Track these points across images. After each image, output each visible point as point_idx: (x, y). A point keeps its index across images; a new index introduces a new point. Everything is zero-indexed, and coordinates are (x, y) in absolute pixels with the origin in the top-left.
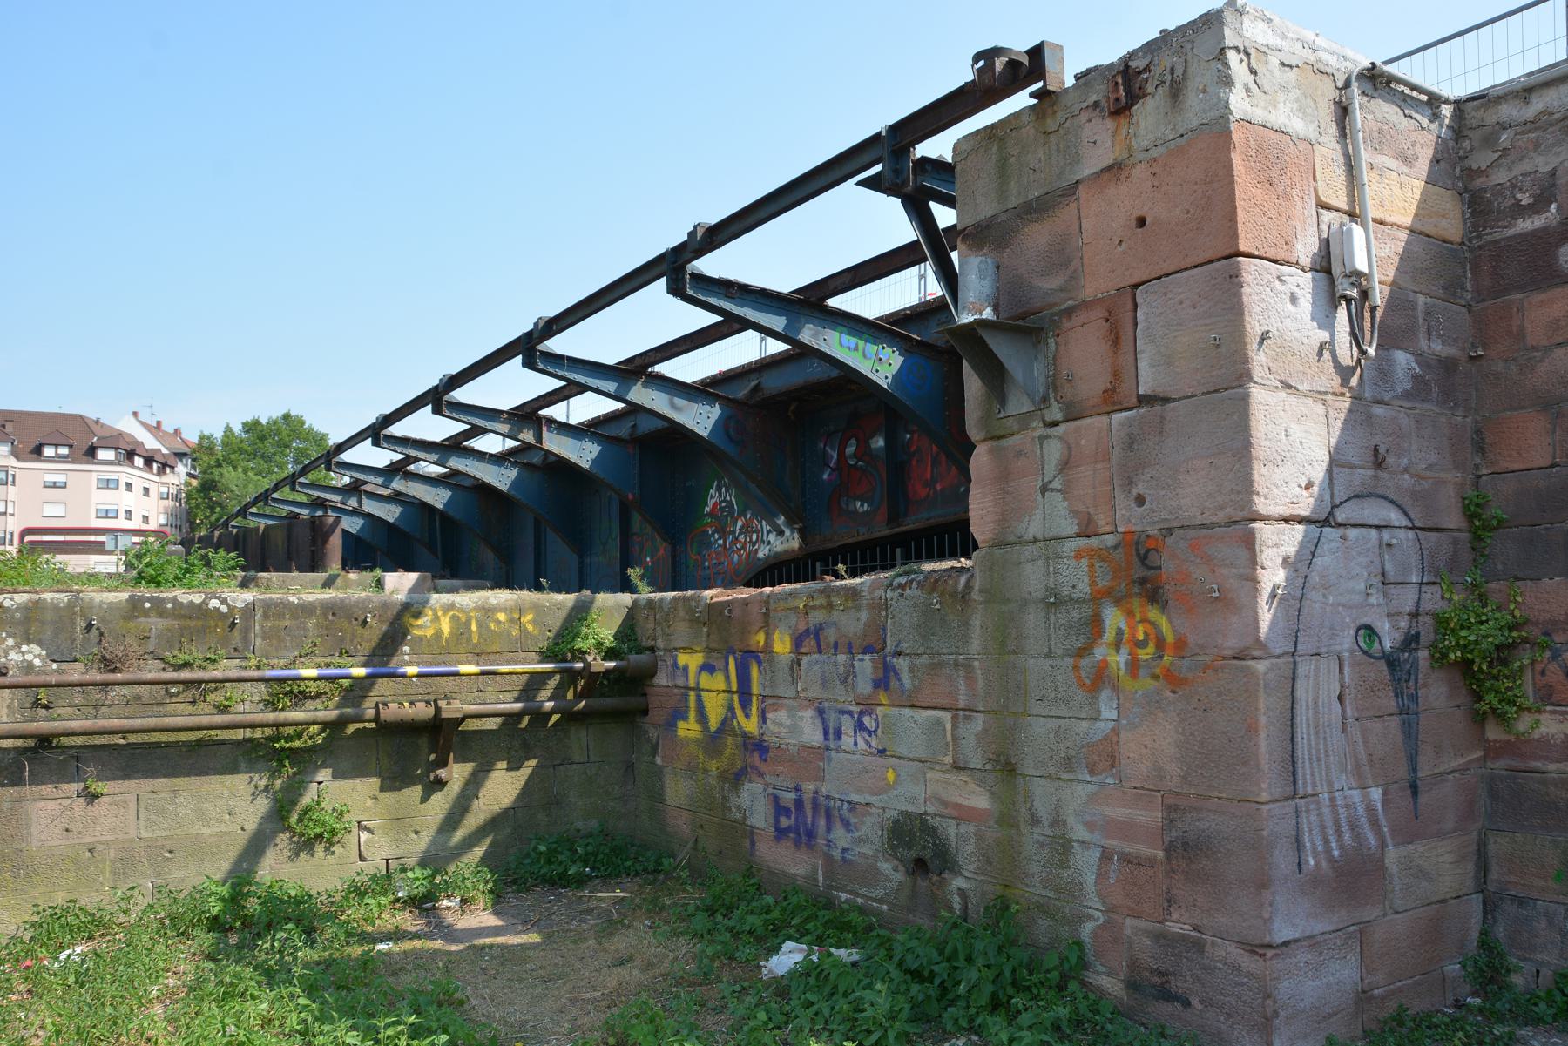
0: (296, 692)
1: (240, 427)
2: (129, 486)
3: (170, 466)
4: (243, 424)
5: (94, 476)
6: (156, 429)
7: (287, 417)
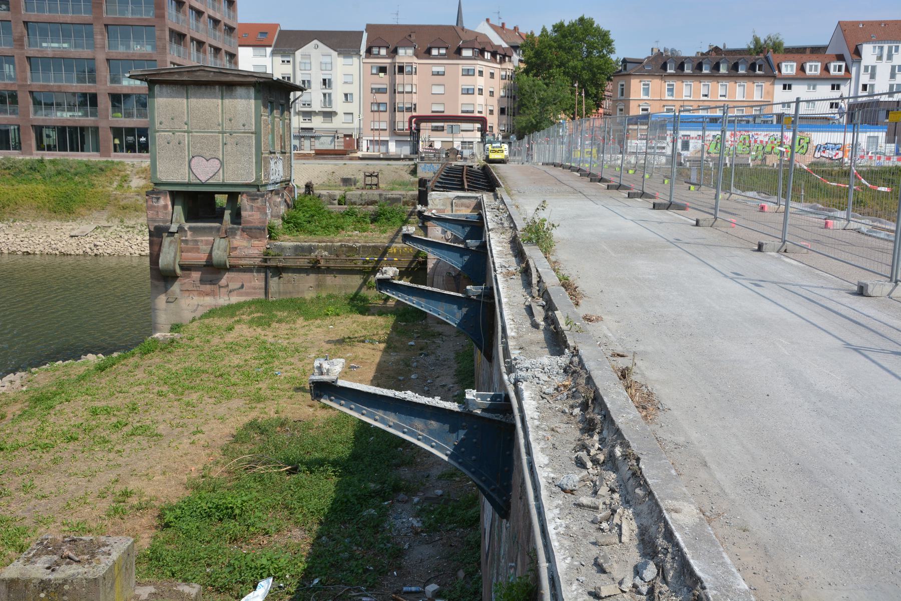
0: (368, 262)
1: (552, 28)
2: (481, 73)
3: (508, 56)
4: (553, 26)
5: (460, 67)
6: (500, 29)
7: (582, 20)
